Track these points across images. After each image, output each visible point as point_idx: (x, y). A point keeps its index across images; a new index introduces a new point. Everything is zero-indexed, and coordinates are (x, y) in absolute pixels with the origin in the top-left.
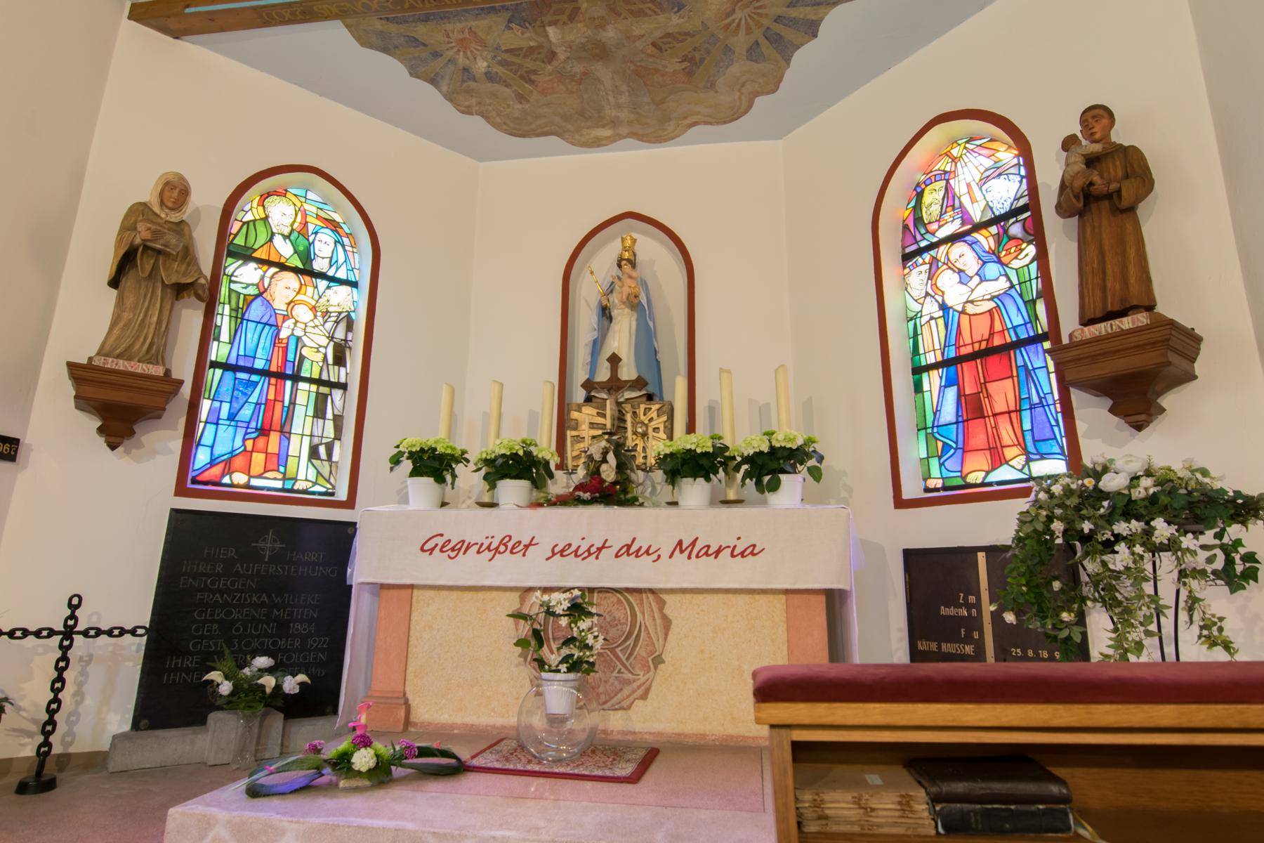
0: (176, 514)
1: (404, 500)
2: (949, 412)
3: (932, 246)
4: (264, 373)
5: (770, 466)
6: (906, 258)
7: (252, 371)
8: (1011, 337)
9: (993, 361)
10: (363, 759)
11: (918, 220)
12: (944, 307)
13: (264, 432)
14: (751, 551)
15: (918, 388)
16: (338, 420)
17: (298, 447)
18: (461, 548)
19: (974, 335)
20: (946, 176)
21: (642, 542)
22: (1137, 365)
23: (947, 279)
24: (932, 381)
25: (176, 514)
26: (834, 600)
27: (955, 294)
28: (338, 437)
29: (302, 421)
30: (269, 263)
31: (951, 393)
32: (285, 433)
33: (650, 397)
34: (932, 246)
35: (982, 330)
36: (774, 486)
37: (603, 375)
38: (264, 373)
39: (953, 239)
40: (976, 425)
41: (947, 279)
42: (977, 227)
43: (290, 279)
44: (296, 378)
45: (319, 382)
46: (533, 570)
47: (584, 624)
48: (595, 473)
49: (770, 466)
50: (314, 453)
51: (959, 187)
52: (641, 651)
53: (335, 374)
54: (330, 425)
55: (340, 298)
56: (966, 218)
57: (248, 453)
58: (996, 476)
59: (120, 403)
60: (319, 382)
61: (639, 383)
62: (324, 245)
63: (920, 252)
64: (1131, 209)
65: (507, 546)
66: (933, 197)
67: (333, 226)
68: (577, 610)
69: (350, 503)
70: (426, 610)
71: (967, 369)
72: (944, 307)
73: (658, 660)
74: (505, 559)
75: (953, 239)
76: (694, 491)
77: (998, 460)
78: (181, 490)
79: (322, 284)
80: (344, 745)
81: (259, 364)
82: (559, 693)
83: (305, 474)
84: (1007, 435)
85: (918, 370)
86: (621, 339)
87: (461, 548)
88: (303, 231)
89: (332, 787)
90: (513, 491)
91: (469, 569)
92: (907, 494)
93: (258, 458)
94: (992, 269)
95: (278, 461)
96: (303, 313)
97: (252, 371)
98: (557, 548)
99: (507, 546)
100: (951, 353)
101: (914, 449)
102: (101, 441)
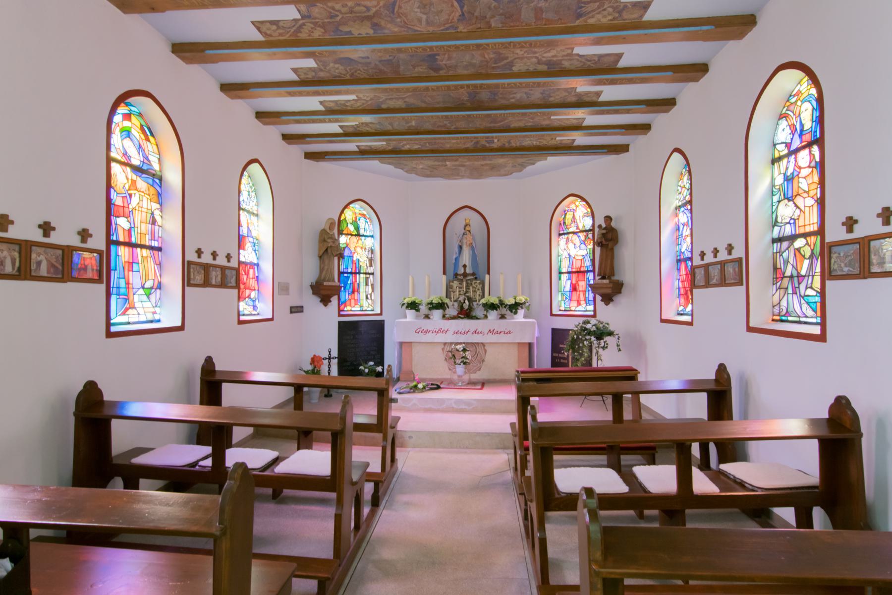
0: (340, 323)
1: (406, 317)
2: (568, 288)
3: (568, 233)
4: (351, 273)
5: (514, 307)
6: (560, 235)
7: (347, 273)
8: (586, 269)
9: (581, 275)
10: (420, 386)
11: (564, 223)
12: (569, 255)
13: (353, 292)
14: (510, 332)
15: (560, 279)
16: (372, 285)
17: (363, 296)
18: (427, 332)
19: (577, 265)
20: (574, 211)
21: (479, 330)
22: (610, 288)
23: (571, 245)
24: (564, 277)
25: (340, 323)
26: (530, 345)
27: (573, 252)
28: (373, 291)
29: (363, 288)
30: (348, 234)
31: (569, 282)
32: (359, 292)
33: (476, 278)
34: (568, 233)
35: (578, 265)
36: (516, 313)
37: (461, 271)
38: (351, 273)
39: (574, 233)
40: (574, 293)
41: (571, 245)
42: (581, 231)
43: (354, 239)
44: (359, 273)
45: (366, 273)
46: (449, 338)
47: (467, 353)
48: (462, 307)
49: (514, 307)
50: (367, 298)
51: (577, 215)
52: (479, 358)
53: (370, 270)
54: (370, 287)
55: (369, 242)
56: (578, 228)
57: (350, 300)
58: (578, 309)
59: (324, 292)
60: (366, 273)
61: (473, 274)
62: (362, 223)
63: (564, 234)
64: (612, 249)
65: (440, 331)
66: (569, 216)
67: (364, 216)
68: (464, 350)
69: (381, 314)
70: (416, 349)
71: (574, 275)
72: (569, 255)
73: (483, 361)
74: (440, 334)
75: (574, 233)
76: (493, 315)
77: (579, 304)
78: (340, 315)
79: (363, 238)
80: (415, 383)
81: (349, 270)
82: (460, 369)
83: (366, 305)
84: (582, 298)
85: (560, 273)
86: (466, 258)
87: (427, 332)
88: (356, 221)
89: (414, 392)
90: (437, 313)
91: (429, 338)
92: (554, 313)
93: (353, 301)
94: (583, 246)
95: (357, 302)
96: (359, 250)
97: (347, 273)
98: (457, 331)
99: (440, 331)
100: (570, 270)
101: (558, 298)
102: (321, 305)
